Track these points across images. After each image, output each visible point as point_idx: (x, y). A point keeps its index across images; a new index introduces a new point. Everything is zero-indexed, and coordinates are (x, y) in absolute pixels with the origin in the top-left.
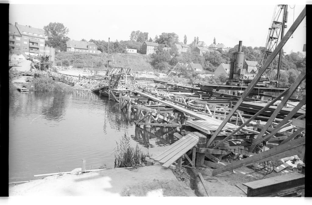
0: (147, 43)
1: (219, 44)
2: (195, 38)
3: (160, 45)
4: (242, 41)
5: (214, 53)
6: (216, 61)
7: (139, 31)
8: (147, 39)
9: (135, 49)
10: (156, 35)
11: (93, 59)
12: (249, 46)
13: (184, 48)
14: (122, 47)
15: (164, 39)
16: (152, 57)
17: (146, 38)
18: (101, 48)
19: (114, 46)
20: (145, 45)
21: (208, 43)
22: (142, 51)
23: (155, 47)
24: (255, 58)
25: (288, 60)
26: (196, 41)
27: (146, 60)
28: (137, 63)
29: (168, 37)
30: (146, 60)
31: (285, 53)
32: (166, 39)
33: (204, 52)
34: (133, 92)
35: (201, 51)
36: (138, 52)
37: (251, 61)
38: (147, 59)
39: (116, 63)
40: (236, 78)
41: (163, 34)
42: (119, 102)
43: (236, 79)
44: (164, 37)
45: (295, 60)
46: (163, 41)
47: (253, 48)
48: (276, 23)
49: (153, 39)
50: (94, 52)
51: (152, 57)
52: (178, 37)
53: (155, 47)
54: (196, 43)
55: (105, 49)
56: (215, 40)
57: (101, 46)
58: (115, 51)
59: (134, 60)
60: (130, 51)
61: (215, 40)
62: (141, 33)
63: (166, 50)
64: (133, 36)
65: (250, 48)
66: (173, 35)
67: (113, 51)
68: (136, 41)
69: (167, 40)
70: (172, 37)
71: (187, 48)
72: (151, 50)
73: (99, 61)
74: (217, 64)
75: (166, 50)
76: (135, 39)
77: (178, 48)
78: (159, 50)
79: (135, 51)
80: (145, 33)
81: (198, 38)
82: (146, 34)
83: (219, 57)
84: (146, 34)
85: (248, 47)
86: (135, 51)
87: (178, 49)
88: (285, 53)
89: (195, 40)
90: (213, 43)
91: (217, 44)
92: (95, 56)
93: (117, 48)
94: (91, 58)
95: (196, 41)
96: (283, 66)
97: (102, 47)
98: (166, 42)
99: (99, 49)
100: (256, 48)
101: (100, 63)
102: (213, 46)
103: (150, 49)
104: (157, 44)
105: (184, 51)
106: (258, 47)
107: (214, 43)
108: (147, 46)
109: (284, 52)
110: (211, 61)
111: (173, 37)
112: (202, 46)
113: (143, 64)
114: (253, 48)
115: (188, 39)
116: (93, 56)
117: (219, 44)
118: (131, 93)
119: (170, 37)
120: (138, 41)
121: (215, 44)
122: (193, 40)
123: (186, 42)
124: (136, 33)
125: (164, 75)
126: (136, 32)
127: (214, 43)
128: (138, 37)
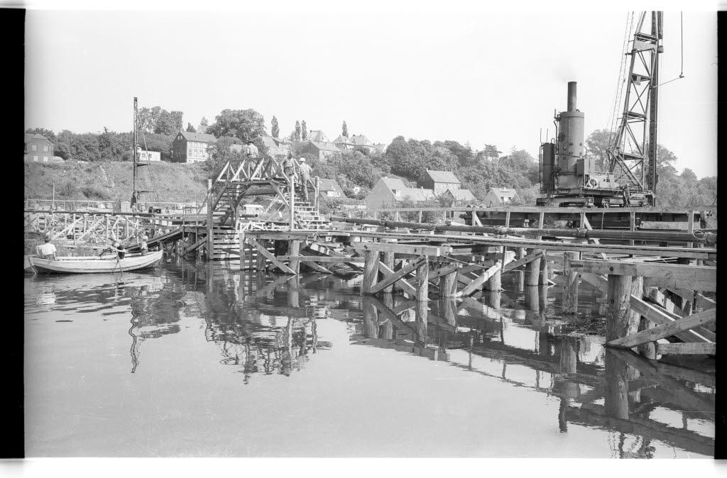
0: (187, 135)
1: (354, 135)
2: (297, 123)
3: (222, 138)
4: (576, 83)
5: (352, 155)
6: (360, 173)
7: (159, 108)
8: (181, 126)
9: (155, 150)
10: (203, 118)
11: (46, 176)
12: (423, 140)
13: (280, 145)
14: (119, 147)
15: (228, 125)
16: (205, 169)
17: (179, 125)
18: (64, 151)
19: (97, 144)
20: (180, 141)
21: (331, 134)
22: (176, 153)
23: (209, 144)
24: (445, 164)
25: (513, 166)
26: (300, 130)
27: (192, 176)
28: (170, 185)
29: (238, 120)
30: (192, 176)
31: (500, 152)
32: (233, 125)
33: (329, 153)
34: (334, 237)
35: (321, 152)
36: (162, 158)
37: (436, 170)
38: (194, 173)
39: (113, 185)
40: (571, 187)
41: (224, 112)
42: (294, 274)
43: (569, 190)
44: (227, 119)
45: (523, 167)
46: (227, 130)
47: (432, 143)
48: (640, 37)
49: (196, 128)
50: (46, 160)
51: (205, 169)
52: (262, 120)
53: (209, 144)
54: (301, 136)
55: (74, 152)
56: (344, 127)
57: (61, 144)
58: (102, 156)
59: (162, 176)
60: (144, 156)
61: (344, 127)
62: (165, 114)
63: (239, 151)
64: (143, 121)
65: (425, 143)
66: (252, 114)
67: (97, 157)
68: (152, 131)
69: (237, 128)
70: (247, 119)
71: (287, 146)
72: (197, 153)
73: (65, 181)
74: (364, 180)
75: (239, 151)
76: (150, 128)
77: (266, 145)
78: (219, 155)
79: (156, 156)
80: (173, 113)
81: (304, 124)
82: (177, 117)
83: (367, 165)
84: (177, 117)
85: (422, 142)
86: (156, 156)
87: (267, 148)
88: (500, 152)
89: (298, 130)
90: (341, 135)
91: (350, 136)
92: (51, 169)
93: (109, 149)
94: (43, 174)
95: (300, 130)
96: (505, 181)
97: (66, 146)
98: (233, 131)
99: (57, 154)
100: (437, 144)
101: (69, 185)
102: (344, 142)
103: (196, 151)
104: (212, 138)
105: (281, 153)
106: (443, 141)
107: (345, 134)
108: (188, 143)
109: (498, 150)
110: (348, 175)
111: (250, 121)
112: (317, 140)
113: (186, 186)
114: (432, 143)
115: (280, 126)
116: (46, 169)
117: (354, 135)
118: (327, 239)
119: (244, 119)
120: (158, 131)
121: (347, 137)
122: (294, 130)
123: (278, 132)
124: (152, 113)
125: (257, 209)
126: (151, 111)
127: (345, 134)
128: (158, 123)
